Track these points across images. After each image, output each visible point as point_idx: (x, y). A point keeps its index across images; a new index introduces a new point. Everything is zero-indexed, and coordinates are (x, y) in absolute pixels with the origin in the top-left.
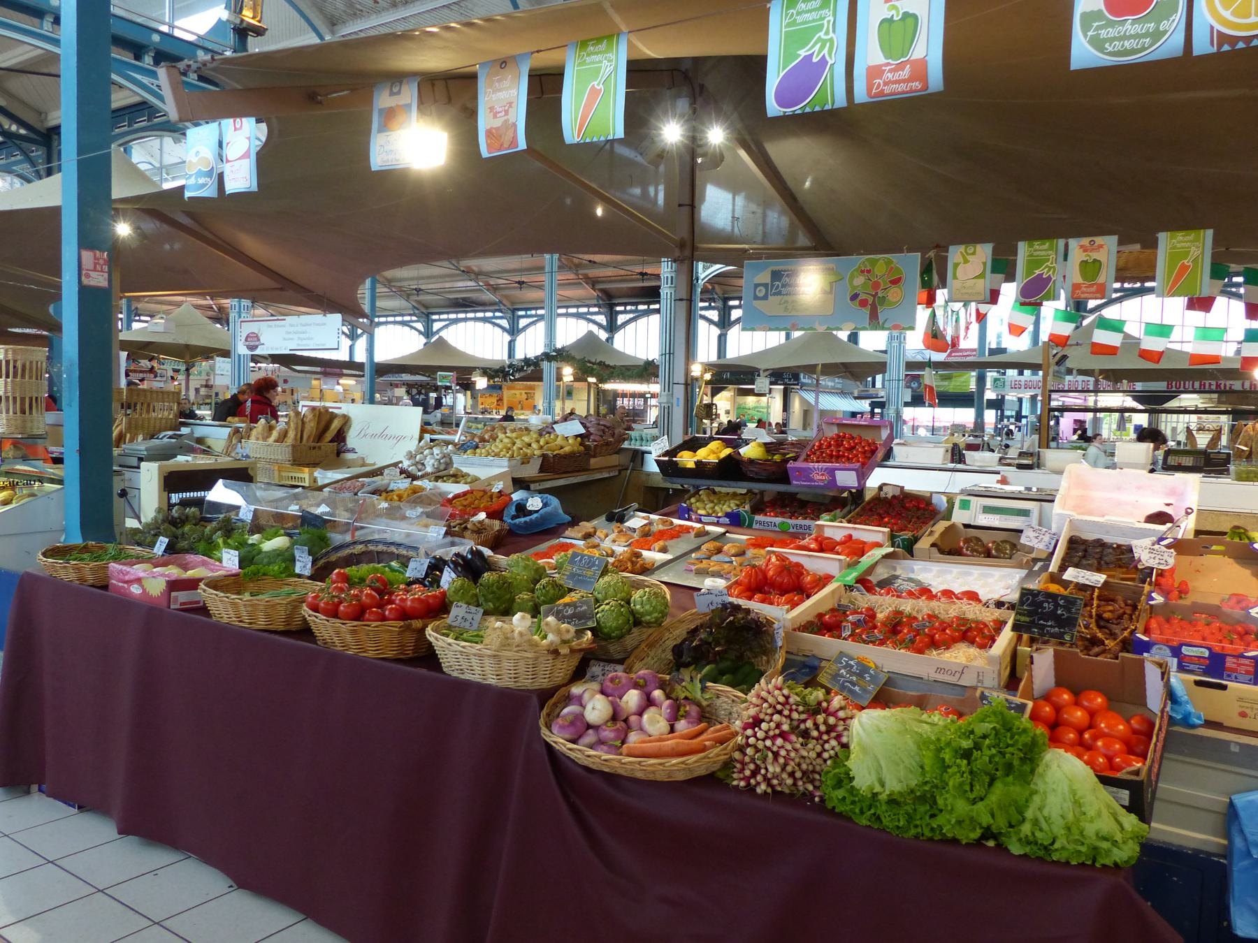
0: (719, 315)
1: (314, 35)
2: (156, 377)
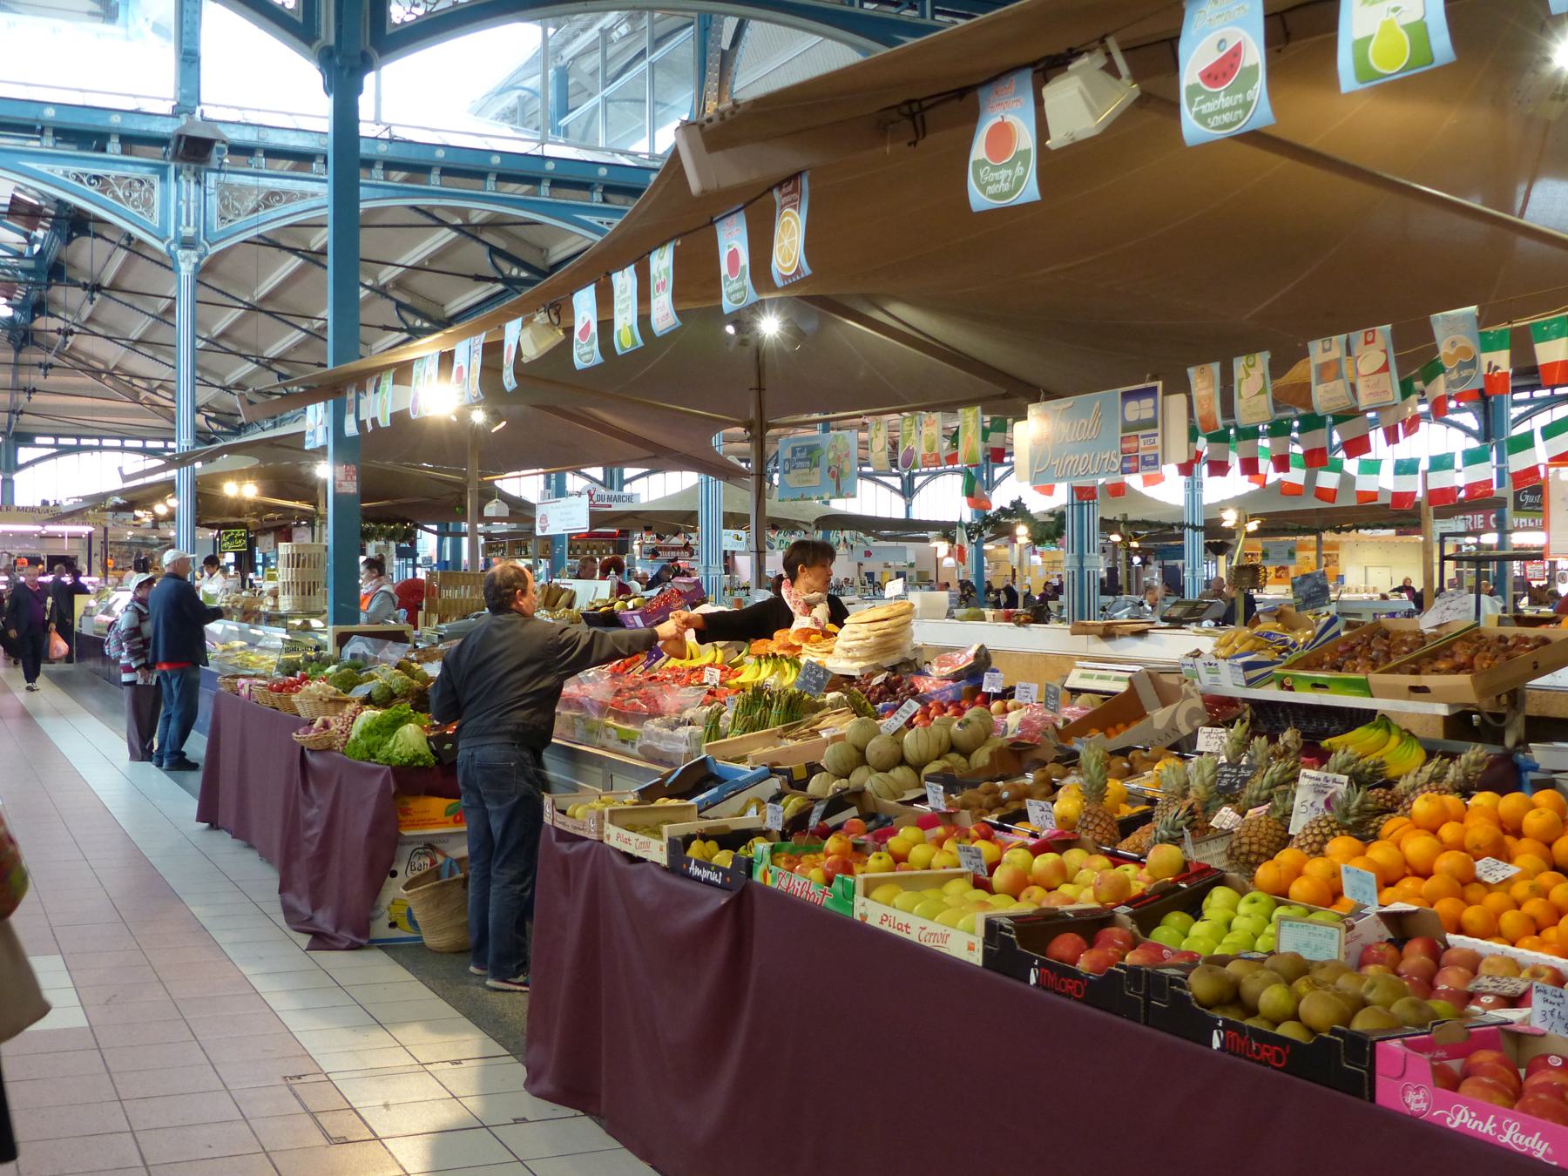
2: (692, 555)
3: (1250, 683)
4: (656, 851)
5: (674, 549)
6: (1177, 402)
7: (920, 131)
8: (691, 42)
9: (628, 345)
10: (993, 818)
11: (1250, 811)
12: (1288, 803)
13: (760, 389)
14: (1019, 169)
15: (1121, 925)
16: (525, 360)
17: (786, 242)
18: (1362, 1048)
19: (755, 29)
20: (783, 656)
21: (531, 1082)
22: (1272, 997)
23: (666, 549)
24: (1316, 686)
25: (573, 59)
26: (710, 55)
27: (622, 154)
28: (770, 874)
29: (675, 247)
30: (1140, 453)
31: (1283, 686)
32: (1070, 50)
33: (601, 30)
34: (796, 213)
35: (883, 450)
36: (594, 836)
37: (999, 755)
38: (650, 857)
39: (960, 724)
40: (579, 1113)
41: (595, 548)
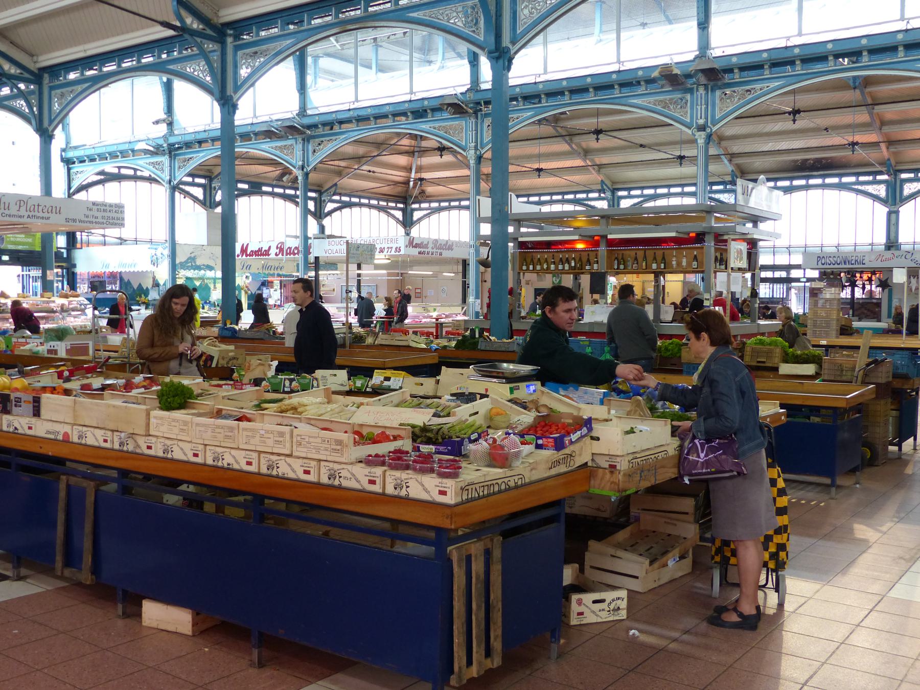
0: (887, 191)
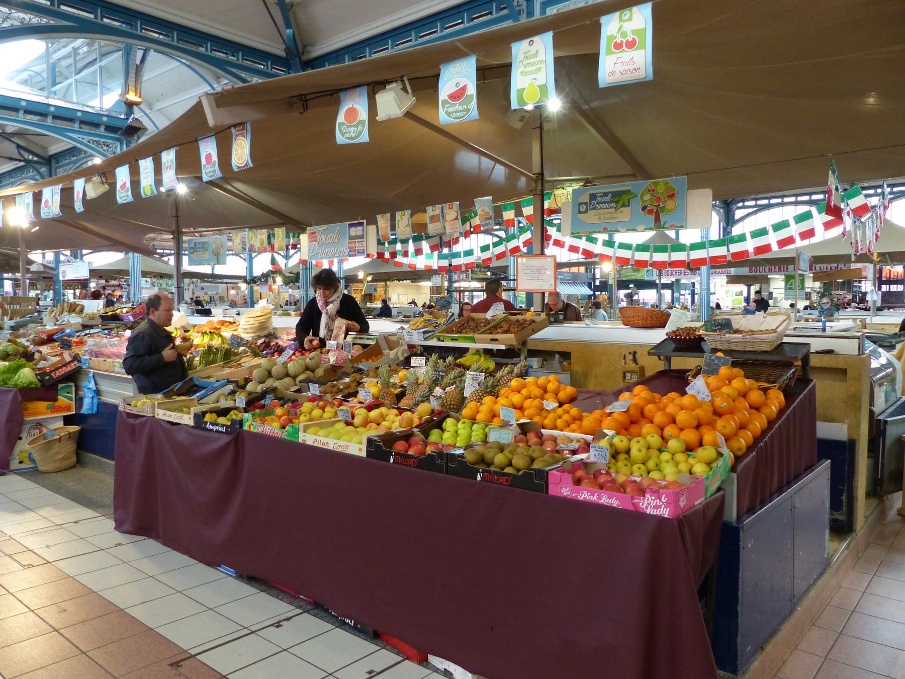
1: (207, 85)
2: (122, 289)
3: (425, 339)
4: (187, 420)
5: (113, 286)
6: (372, 228)
7: (305, 108)
8: (121, 59)
9: (149, 193)
10: (339, 397)
11: (447, 389)
12: (462, 385)
13: (177, 216)
14: (360, 128)
15: (417, 436)
16: (88, 198)
17: (240, 152)
18: (543, 475)
19: (152, 56)
20: (213, 332)
21: (119, 527)
22: (499, 459)
23: (110, 286)
24: (453, 340)
25: (58, 60)
26: (130, 66)
27: (88, 106)
28: (251, 424)
29: (176, 150)
30: (357, 249)
31: (439, 340)
32: (386, 80)
33: (73, 48)
34: (245, 139)
35: (239, 244)
36: (151, 415)
37: (326, 371)
38: (183, 422)
39: (310, 359)
40: (146, 538)
41: (72, 286)
